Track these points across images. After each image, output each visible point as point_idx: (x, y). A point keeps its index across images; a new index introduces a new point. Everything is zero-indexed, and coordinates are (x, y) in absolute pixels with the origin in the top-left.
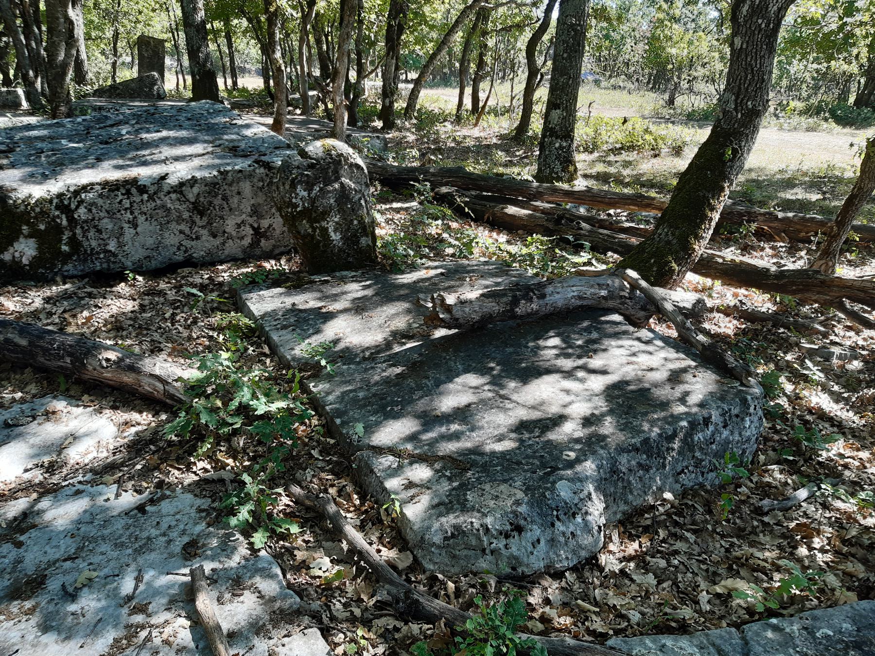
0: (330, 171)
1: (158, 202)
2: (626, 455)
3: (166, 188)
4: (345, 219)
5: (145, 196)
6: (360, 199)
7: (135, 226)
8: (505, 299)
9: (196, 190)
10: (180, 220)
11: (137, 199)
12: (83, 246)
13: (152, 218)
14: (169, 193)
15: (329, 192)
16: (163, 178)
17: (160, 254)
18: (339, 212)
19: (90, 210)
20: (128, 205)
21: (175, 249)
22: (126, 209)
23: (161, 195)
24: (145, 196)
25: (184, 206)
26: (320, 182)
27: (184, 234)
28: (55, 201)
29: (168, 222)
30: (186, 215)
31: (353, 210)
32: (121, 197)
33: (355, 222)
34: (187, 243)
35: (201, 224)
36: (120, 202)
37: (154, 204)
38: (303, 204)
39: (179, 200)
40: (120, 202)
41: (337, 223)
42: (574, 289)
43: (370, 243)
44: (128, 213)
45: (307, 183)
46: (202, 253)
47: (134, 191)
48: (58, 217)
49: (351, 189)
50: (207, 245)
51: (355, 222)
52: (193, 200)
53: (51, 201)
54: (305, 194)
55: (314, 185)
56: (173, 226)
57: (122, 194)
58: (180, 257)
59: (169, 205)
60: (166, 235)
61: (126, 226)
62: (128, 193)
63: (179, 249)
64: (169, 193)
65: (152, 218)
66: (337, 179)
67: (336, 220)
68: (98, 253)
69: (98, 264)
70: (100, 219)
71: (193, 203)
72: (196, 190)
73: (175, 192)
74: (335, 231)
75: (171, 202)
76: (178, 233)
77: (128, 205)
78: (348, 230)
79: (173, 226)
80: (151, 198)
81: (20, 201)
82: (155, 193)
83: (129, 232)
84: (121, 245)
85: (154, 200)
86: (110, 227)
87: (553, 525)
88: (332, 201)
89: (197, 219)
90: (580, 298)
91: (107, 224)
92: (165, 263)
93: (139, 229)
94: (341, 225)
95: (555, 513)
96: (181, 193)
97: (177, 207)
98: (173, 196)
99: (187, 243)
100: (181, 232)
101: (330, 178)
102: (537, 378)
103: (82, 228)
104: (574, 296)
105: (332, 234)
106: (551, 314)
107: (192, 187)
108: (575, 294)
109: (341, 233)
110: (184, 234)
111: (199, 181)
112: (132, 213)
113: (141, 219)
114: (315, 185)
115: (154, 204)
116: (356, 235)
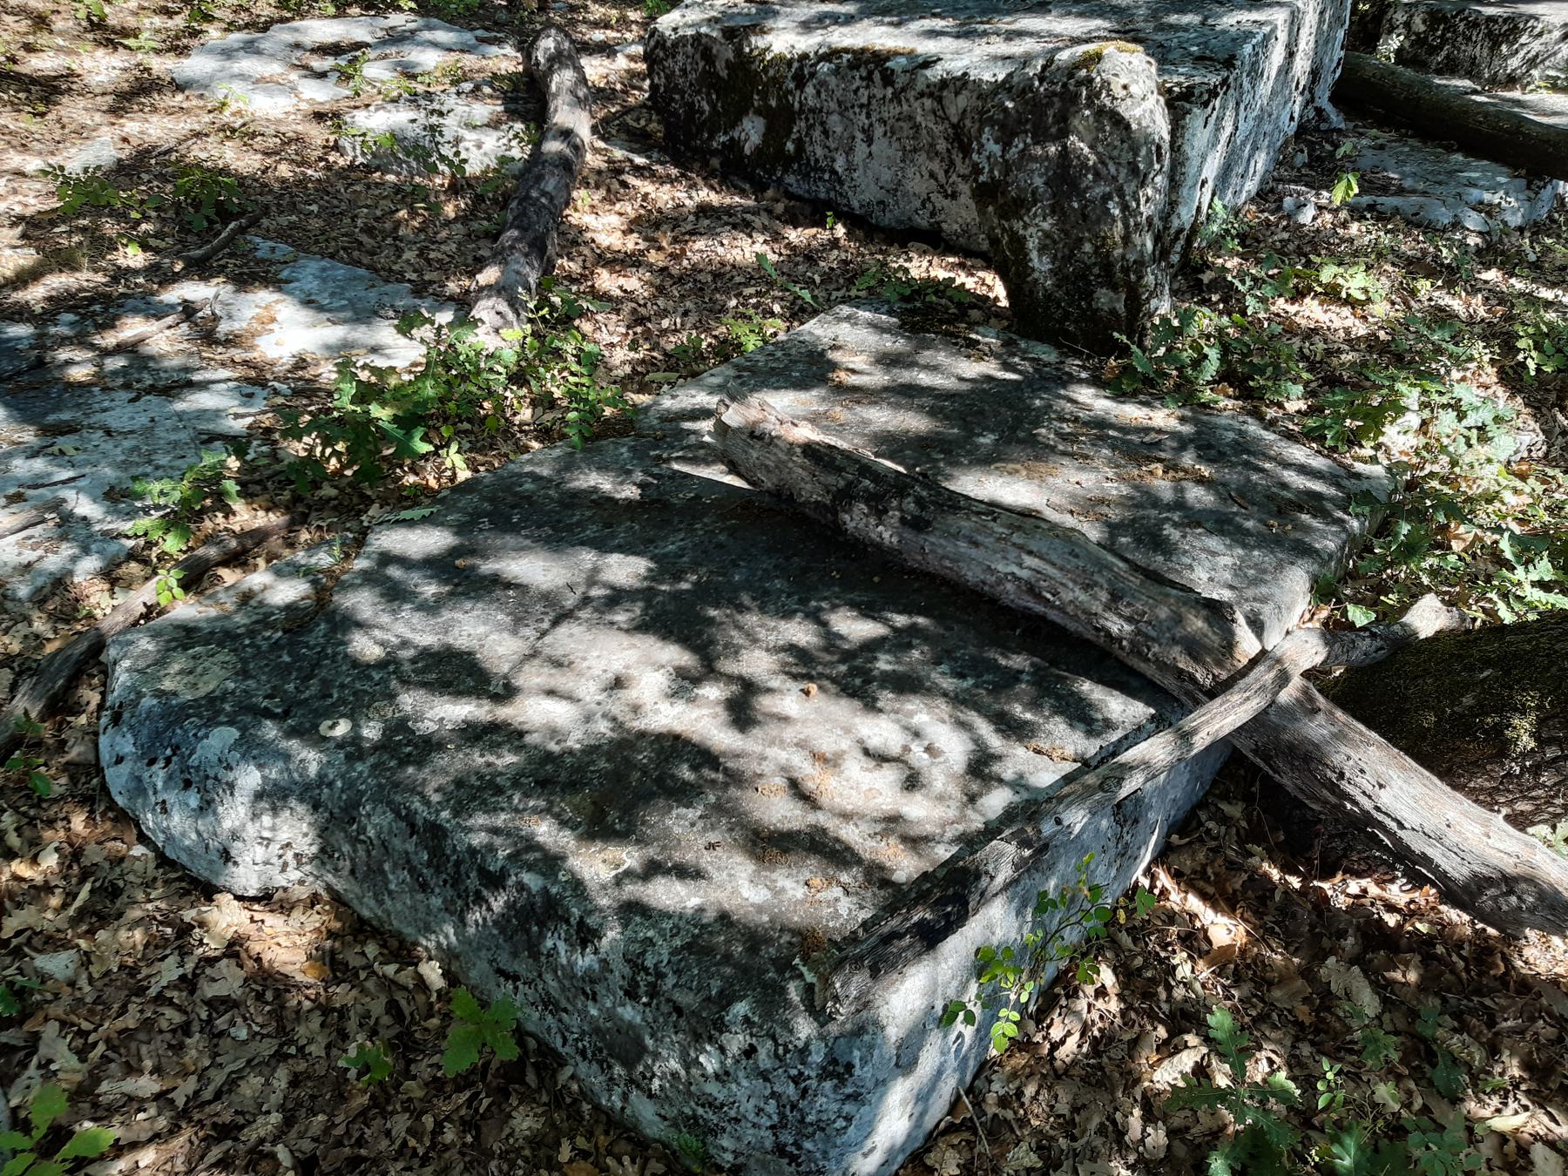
0: (1050, 112)
1: (905, 107)
2: (390, 816)
3: (920, 85)
4: (1067, 234)
5: (890, 91)
6: (1106, 198)
7: (869, 141)
8: (831, 479)
9: (962, 101)
10: (932, 153)
11: (878, 92)
12: (1081, 195)
13: (893, 133)
14: (922, 95)
15: (1035, 159)
16: (928, 63)
17: (897, 203)
18: (1053, 212)
19: (819, 93)
20: (864, 100)
21: (918, 204)
22: (861, 106)
23: (911, 94)
24: (890, 91)
25: (941, 128)
26: (1026, 132)
27: (936, 180)
28: (796, 65)
29: (915, 150)
30: (942, 146)
31: (1085, 217)
32: (858, 83)
33: (1088, 247)
34: (939, 201)
35: (962, 171)
36: (856, 91)
37: (898, 109)
38: (991, 171)
39: (934, 113)
40: (856, 91)
41: (1047, 235)
42: (1029, 561)
43: (1120, 307)
44: (863, 117)
45: (1003, 127)
46: (956, 227)
47: (877, 76)
48: (790, 92)
49: (1084, 165)
50: (964, 214)
51: (1088, 247)
52: (955, 120)
53: (790, 63)
54: (995, 149)
55: (1014, 134)
56: (921, 158)
57: (861, 78)
58: (922, 221)
59: (919, 119)
60: (910, 172)
61: (859, 136)
62: (869, 78)
63: (923, 204)
64: (922, 95)
65: (893, 133)
66: (1064, 133)
67: (1045, 226)
68: (823, 171)
69: (823, 190)
70: (828, 113)
71: (954, 126)
72: (962, 101)
73: (931, 95)
74: (1042, 249)
75: (921, 110)
76: (927, 176)
77: (864, 100)
78: (1069, 258)
79: (921, 158)
80: (896, 97)
81: (756, 53)
82: (903, 90)
83: (861, 149)
84: (851, 168)
85: (900, 103)
86: (839, 129)
87: (152, 762)
88: (1038, 182)
89: (958, 158)
90: (1032, 590)
91: (834, 122)
92: (902, 222)
93: (873, 147)
94: (1055, 242)
95: (169, 752)
96: (940, 100)
97: (931, 125)
98: (928, 103)
99: (939, 201)
100: (932, 175)
101: (1047, 129)
102: (664, 638)
103: (807, 119)
104: (1016, 578)
105: (1034, 255)
106: (945, 581)
107: (957, 94)
108: (1024, 574)
109: (1054, 259)
110: (936, 180)
111: (970, 86)
112: (868, 116)
113: (879, 131)
114: (1017, 135)
115: (898, 109)
116: (1084, 277)
